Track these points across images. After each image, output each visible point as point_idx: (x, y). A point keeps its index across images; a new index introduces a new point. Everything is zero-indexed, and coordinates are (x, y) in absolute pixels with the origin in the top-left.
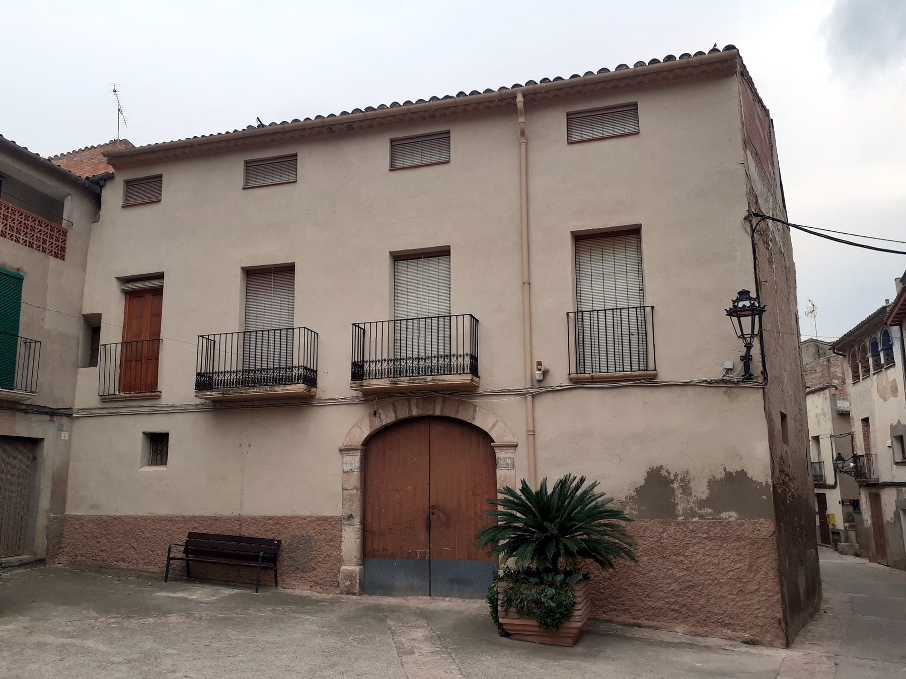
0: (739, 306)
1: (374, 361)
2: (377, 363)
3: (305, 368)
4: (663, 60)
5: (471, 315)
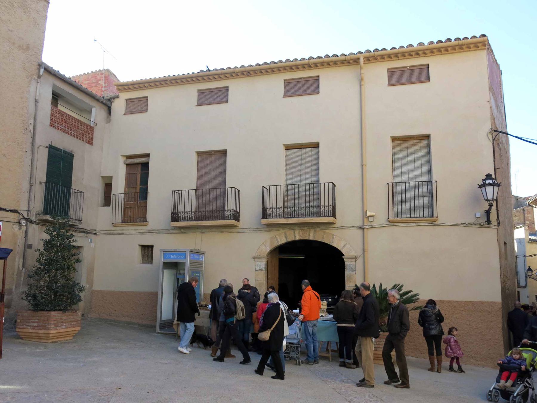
0: (486, 183)
1: (276, 208)
2: (277, 209)
3: (234, 211)
4: (445, 41)
5: (333, 183)
